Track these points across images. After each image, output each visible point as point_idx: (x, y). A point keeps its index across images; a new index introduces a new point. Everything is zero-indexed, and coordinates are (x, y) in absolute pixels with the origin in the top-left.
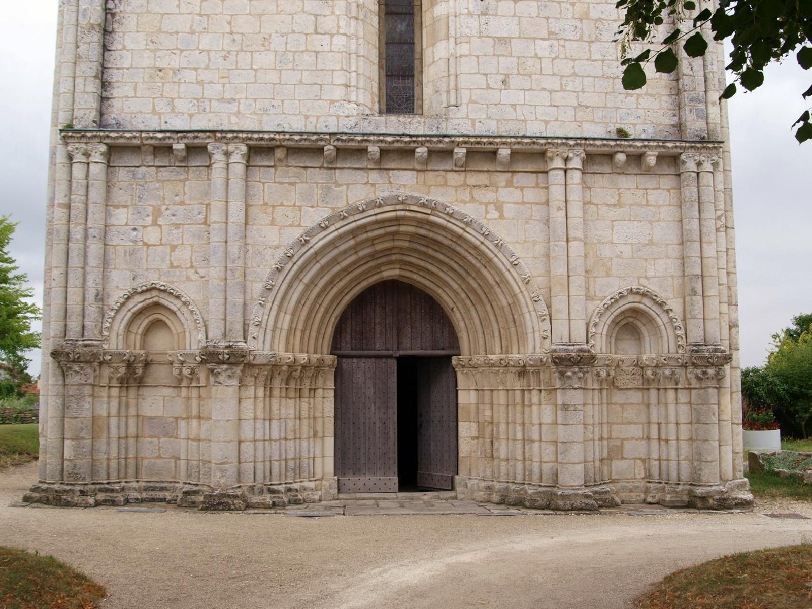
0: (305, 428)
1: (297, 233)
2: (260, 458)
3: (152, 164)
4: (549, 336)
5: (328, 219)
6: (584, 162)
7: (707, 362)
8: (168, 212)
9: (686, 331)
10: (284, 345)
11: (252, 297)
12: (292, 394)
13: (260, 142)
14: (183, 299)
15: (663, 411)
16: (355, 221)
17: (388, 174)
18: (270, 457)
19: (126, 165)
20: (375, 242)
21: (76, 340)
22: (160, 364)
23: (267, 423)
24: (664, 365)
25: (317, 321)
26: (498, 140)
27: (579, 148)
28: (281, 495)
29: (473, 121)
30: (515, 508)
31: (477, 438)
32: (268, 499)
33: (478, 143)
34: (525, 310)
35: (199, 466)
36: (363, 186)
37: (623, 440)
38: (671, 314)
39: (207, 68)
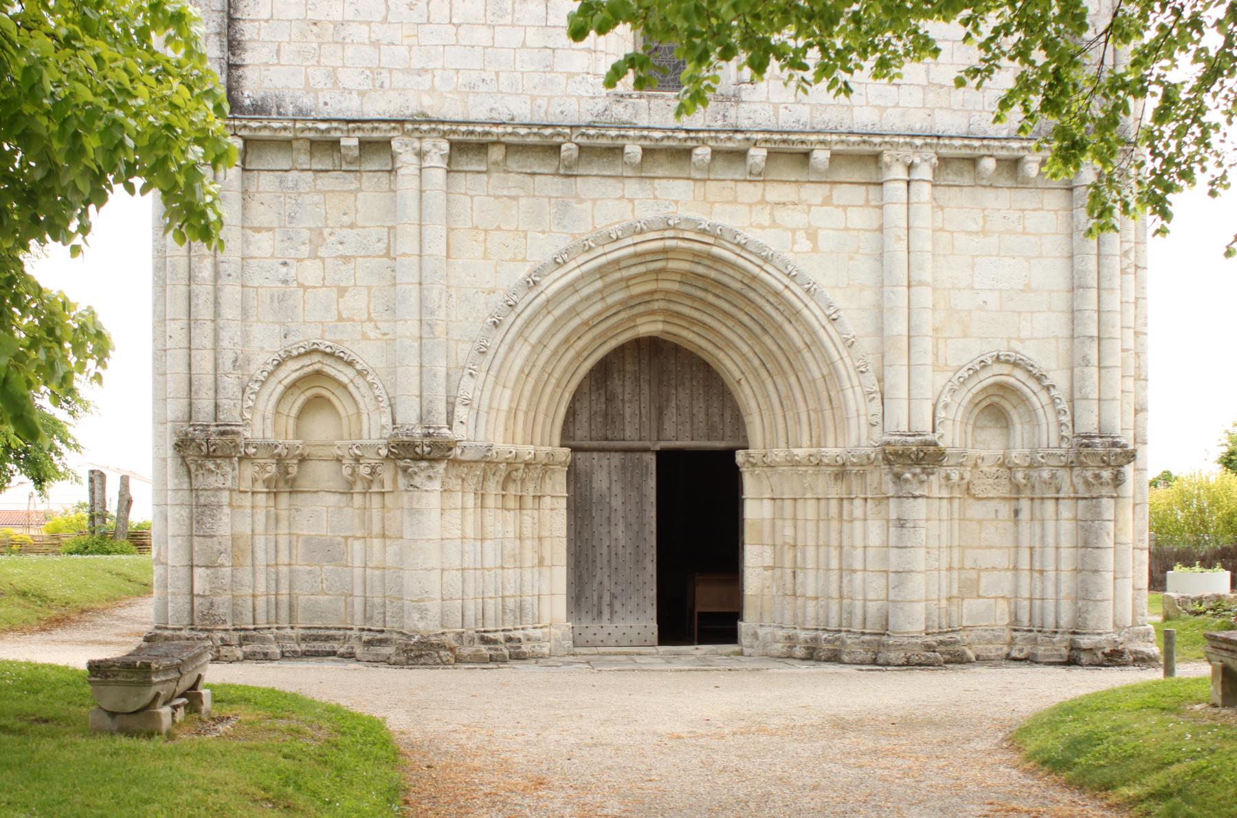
1: (523, 271)
3: (307, 167)
4: (880, 421)
5: (567, 251)
6: (936, 171)
7: (1101, 461)
8: (333, 238)
9: (1073, 416)
12: (511, 503)
14: (358, 367)
15: (1038, 530)
17: (652, 185)
19: (270, 167)
20: (631, 283)
21: (208, 426)
22: (320, 459)
23: (479, 543)
24: (1041, 465)
25: (546, 399)
26: (813, 138)
27: (929, 149)
29: (776, 106)
31: (773, 568)
33: (784, 141)
34: (846, 384)
35: (384, 605)
37: (980, 570)
38: (1053, 392)
39: (385, 20)
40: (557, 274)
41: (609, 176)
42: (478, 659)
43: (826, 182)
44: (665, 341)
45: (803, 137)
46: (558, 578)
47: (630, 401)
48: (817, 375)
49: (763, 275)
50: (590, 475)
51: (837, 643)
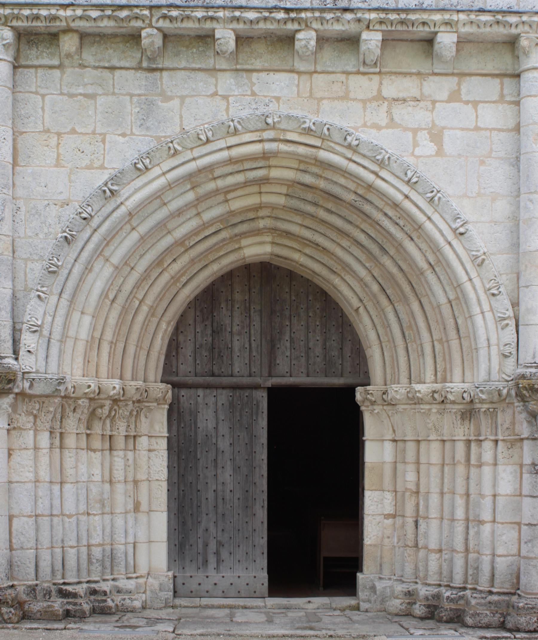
0: (120, 498)
2: (45, 542)
4: (514, 352)
10: (81, 365)
11: (26, 285)
12: (97, 444)
13: (35, 24)
16: (194, 159)
18: (63, 541)
20: (229, 196)
23: (56, 488)
25: (137, 328)
26: (437, 17)
28: (79, 601)
30: (451, 625)
31: (394, 516)
32: (58, 605)
34: (476, 310)
36: (209, 100)
40: (139, 183)
41: (199, 70)
42: (49, 616)
43: (453, 74)
44: (278, 268)
45: (425, 17)
46: (159, 523)
47: (239, 334)
48: (443, 300)
49: (379, 183)
50: (194, 414)
51: (462, 602)
